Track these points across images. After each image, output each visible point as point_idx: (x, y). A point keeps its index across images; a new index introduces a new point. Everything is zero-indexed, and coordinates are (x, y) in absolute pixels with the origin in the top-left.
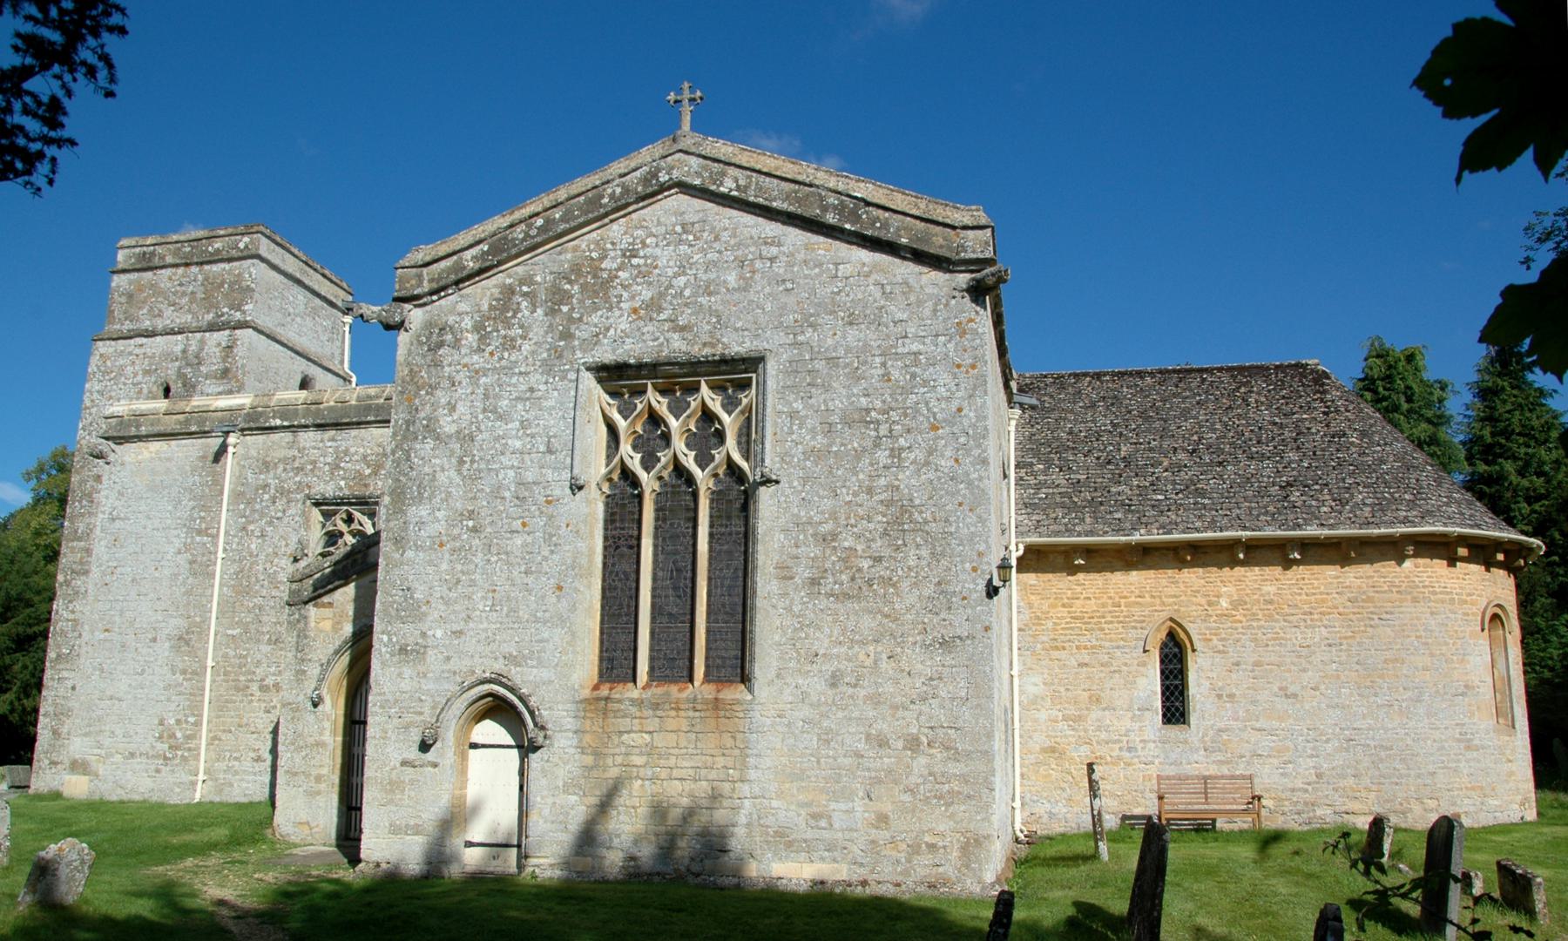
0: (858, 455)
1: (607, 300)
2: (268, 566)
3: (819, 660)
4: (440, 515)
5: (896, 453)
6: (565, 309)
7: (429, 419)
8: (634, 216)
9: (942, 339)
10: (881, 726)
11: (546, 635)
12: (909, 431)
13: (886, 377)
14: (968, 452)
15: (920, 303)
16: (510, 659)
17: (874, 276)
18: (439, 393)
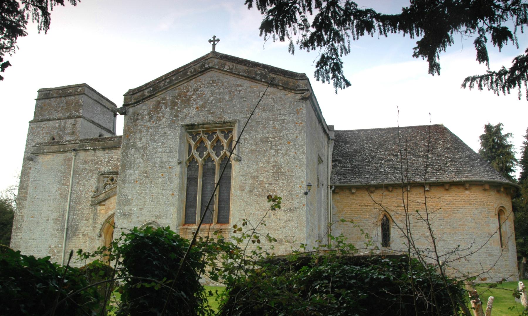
0: (265, 152)
1: (189, 104)
3: (252, 215)
4: (136, 172)
5: (277, 151)
6: (176, 108)
7: (133, 142)
8: (198, 78)
9: (292, 115)
11: (168, 209)
12: (281, 144)
13: (274, 127)
14: (299, 150)
15: (285, 104)
16: (157, 216)
17: (271, 96)
18: (137, 135)
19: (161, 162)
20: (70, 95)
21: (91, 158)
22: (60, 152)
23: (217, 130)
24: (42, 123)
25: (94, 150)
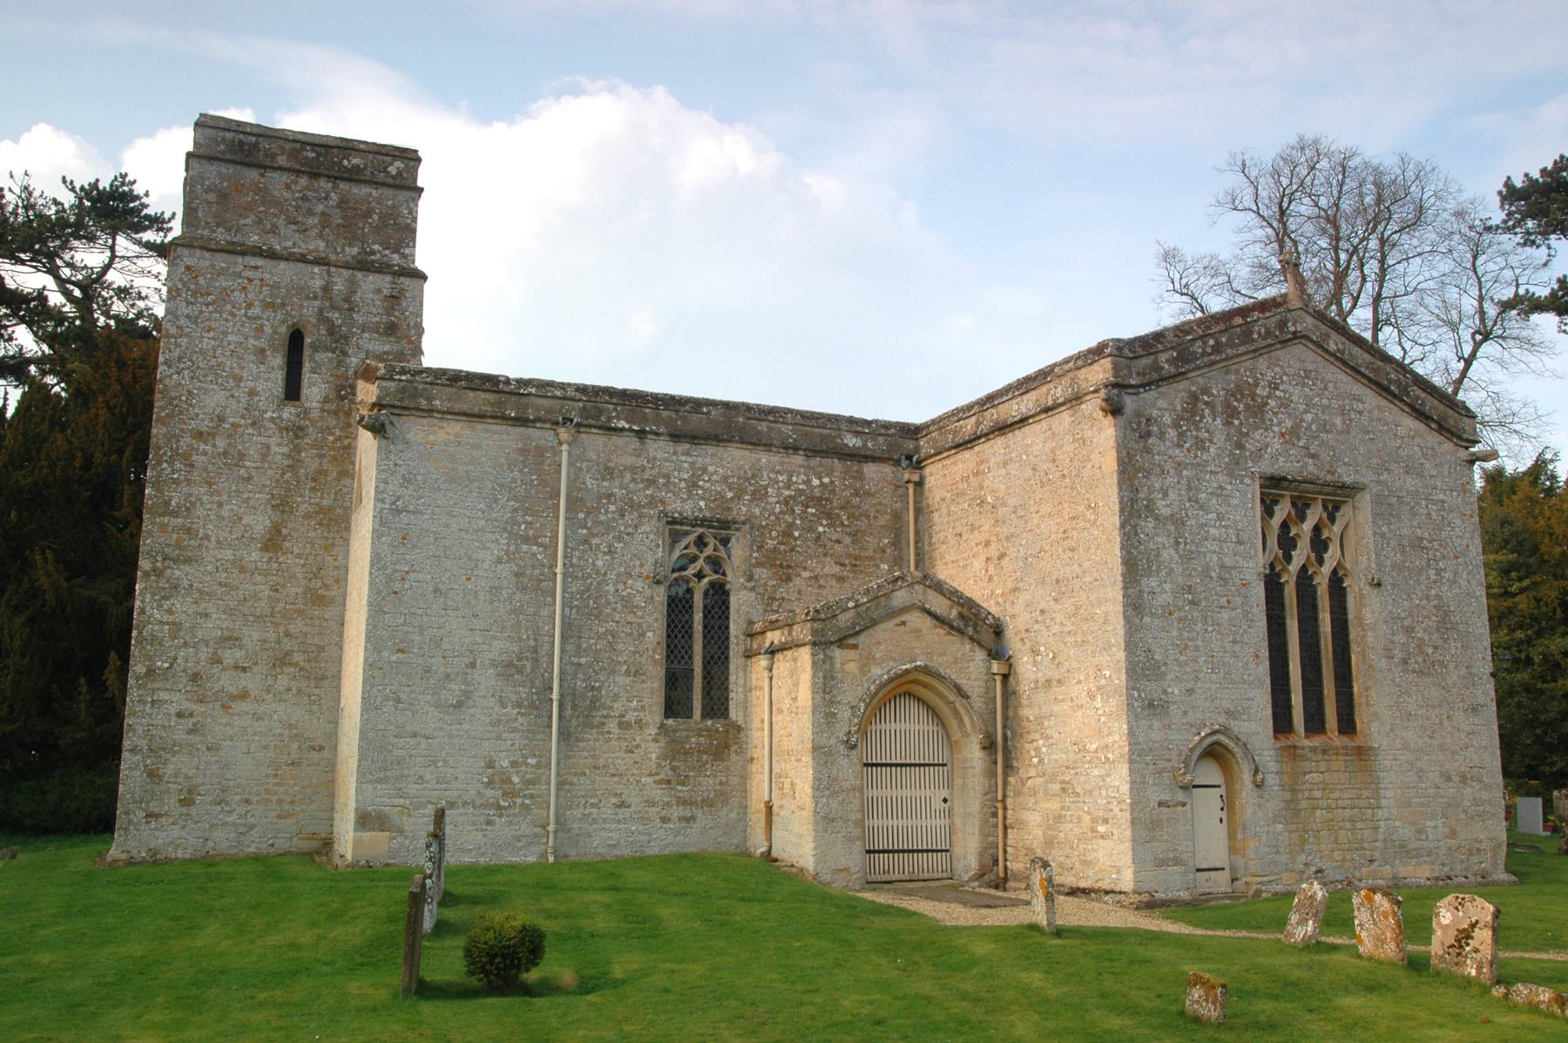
0: (1420, 571)
1: (1263, 419)
2: (621, 587)
4: (1167, 586)
10: (1447, 766)
11: (1251, 695)
18: (1153, 478)
19: (1222, 567)
20: (354, 176)
21: (629, 460)
22: (505, 418)
23: (1283, 496)
24: (240, 259)
25: (641, 434)
